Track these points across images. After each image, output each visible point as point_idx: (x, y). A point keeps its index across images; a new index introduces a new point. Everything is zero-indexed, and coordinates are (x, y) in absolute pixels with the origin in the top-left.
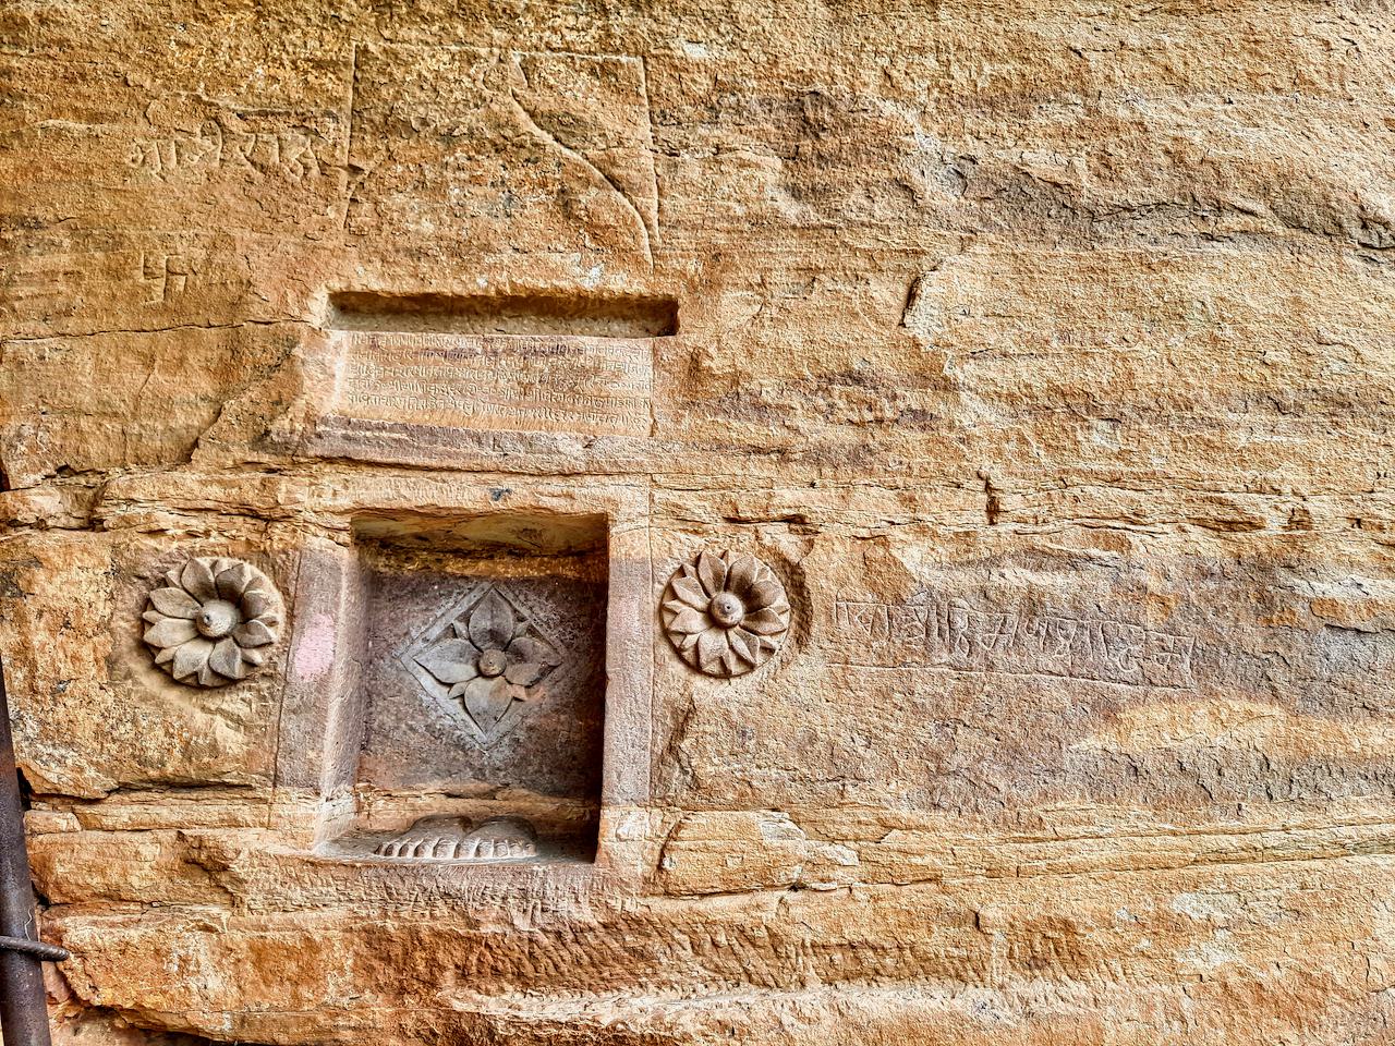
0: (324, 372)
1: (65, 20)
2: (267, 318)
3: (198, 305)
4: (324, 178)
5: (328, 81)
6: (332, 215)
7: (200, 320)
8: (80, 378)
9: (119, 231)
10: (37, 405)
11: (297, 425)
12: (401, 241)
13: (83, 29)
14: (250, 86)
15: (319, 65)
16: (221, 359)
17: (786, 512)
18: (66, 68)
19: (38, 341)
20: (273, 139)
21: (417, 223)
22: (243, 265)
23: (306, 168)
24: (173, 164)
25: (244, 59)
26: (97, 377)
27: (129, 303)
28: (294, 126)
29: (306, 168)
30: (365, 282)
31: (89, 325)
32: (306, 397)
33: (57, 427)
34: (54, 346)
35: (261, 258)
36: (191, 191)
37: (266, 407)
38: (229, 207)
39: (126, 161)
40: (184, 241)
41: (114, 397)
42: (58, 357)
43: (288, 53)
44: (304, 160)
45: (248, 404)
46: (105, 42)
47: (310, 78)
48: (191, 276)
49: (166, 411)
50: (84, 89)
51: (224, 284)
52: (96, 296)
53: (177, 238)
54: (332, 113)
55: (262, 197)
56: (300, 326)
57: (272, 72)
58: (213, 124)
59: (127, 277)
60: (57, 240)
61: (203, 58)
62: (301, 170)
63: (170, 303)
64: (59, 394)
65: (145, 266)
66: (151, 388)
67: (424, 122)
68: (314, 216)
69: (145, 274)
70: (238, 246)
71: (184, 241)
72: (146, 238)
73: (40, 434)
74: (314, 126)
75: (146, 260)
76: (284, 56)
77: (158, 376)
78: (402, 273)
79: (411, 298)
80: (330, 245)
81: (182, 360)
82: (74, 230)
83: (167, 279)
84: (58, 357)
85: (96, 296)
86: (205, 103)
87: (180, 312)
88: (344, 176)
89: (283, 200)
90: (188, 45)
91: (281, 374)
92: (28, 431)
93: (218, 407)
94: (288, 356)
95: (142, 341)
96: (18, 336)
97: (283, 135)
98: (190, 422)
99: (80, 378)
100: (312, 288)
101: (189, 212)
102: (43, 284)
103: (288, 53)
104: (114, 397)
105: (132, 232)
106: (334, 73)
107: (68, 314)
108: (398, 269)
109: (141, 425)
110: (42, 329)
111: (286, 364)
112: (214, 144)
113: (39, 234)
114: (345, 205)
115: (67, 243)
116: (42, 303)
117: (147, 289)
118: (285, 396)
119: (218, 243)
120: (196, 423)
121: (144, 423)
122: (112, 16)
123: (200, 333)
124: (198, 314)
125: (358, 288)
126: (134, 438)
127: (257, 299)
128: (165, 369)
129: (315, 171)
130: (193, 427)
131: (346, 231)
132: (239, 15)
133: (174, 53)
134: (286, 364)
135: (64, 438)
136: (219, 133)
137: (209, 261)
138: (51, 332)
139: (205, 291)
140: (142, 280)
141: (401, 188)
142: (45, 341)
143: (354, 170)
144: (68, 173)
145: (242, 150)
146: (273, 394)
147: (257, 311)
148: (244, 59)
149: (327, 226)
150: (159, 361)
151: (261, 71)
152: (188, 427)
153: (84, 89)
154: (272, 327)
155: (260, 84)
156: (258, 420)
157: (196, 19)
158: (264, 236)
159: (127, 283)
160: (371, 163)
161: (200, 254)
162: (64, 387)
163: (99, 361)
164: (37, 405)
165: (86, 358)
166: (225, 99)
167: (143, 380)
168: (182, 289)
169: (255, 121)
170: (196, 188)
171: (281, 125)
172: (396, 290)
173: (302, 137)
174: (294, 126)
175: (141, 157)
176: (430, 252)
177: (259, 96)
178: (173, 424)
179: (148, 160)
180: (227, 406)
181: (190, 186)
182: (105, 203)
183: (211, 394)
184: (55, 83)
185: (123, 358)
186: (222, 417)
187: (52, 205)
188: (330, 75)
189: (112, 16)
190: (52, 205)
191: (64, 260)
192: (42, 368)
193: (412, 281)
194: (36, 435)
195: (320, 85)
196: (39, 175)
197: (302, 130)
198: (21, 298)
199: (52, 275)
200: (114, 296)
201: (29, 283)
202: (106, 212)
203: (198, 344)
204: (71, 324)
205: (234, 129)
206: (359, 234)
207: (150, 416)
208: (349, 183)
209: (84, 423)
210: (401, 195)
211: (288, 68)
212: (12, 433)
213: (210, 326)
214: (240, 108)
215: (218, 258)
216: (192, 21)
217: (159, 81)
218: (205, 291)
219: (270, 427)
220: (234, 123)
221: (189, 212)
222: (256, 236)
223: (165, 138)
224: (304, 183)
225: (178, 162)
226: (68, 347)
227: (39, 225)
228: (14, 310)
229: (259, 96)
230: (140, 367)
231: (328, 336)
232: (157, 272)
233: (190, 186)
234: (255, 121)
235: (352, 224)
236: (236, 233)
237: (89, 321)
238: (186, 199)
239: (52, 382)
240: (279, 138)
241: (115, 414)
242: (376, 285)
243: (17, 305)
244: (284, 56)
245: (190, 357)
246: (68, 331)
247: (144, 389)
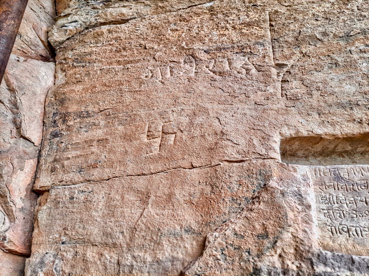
0: (302, 203)
1: (120, 30)
2: (240, 158)
3: (184, 153)
4: (260, 73)
5: (255, 30)
6: (271, 90)
7: (187, 164)
8: (94, 213)
9: (134, 112)
10: (60, 236)
11: (289, 263)
12: (330, 99)
13: (127, 32)
14: (210, 40)
15: (248, 25)
16: (202, 194)
17: (310, 267)
18: (117, 48)
19: (73, 186)
20: (225, 60)
21: (340, 87)
22: (216, 123)
23: (247, 70)
24: (168, 75)
25: (206, 30)
26: (106, 212)
27: (135, 156)
28: (237, 53)
29: (247, 70)
30: (309, 129)
31: (107, 172)
32: (291, 229)
33: (69, 256)
34: (81, 189)
35: (226, 117)
36: (179, 88)
37: (251, 240)
38: (202, 93)
39: (142, 77)
40: (175, 114)
41: (115, 229)
42: (82, 197)
43: (230, 24)
44: (246, 66)
45: (232, 237)
46: (137, 35)
47: (243, 31)
48: (179, 134)
49: (155, 242)
50: (124, 53)
51: (203, 136)
52: (115, 153)
53: (170, 112)
54: (260, 42)
55: (223, 86)
56: (268, 162)
57: (221, 32)
58: (191, 57)
59: (136, 139)
60: (97, 122)
61: (184, 33)
62: (244, 71)
63: (163, 154)
64: (77, 227)
65: (149, 131)
66: (144, 220)
67: (325, 34)
68: (259, 93)
69: (148, 136)
70: (210, 112)
71: (175, 114)
72: (150, 115)
73: (57, 261)
74: (249, 50)
75: (149, 127)
76: (228, 25)
77: (151, 210)
78: (339, 120)
79: (350, 139)
80: (275, 107)
81: (170, 196)
82: (108, 115)
83: (163, 138)
84: (82, 197)
85: (115, 153)
86: (186, 49)
87: (171, 158)
88: (274, 71)
89: (236, 86)
90: (177, 30)
91: (262, 206)
92: (49, 259)
93: (201, 239)
94: (265, 187)
95: (141, 183)
96: (61, 184)
97: (231, 57)
98: (175, 254)
99: (94, 213)
100: (271, 134)
101: (178, 98)
102: (84, 148)
103: (230, 24)
104: (115, 229)
105: (142, 113)
106: (257, 26)
107: (95, 167)
108: (335, 118)
109: (134, 257)
110: (77, 177)
111: (265, 196)
112: (191, 66)
113: (87, 120)
114: (279, 85)
115: (102, 123)
116: (80, 160)
117: (149, 145)
118: (270, 229)
119: (197, 112)
120: (180, 256)
121: (136, 254)
122: (141, 26)
123: (185, 173)
124: (184, 159)
125: (305, 134)
126: (126, 270)
127: (230, 143)
128: (157, 204)
129: (254, 71)
130: (178, 259)
131: (285, 98)
132: (201, 17)
133: (169, 34)
134: (265, 196)
135: (73, 267)
136: (194, 61)
137: (191, 123)
138: (81, 179)
139: (189, 143)
140: (146, 140)
141: (319, 69)
142: (77, 186)
143: (280, 66)
144: (109, 86)
145: (207, 67)
146: (257, 226)
147: (232, 153)
148: (206, 30)
149: (270, 97)
150: (153, 197)
151: (215, 33)
152: (173, 260)
153: (124, 53)
154: (245, 164)
155: (215, 38)
156: (245, 255)
157: (181, 21)
158: (227, 106)
159: (136, 143)
160: (292, 61)
161: (185, 120)
162: (81, 221)
163: (109, 199)
164: (60, 236)
165: (101, 196)
166: (197, 46)
167: (138, 214)
168: (172, 143)
169: (214, 53)
170: (182, 86)
171: (229, 53)
172: (338, 132)
173: (242, 58)
174: (237, 53)
175: (151, 74)
176: (360, 103)
177: (215, 43)
178: (160, 256)
179: (155, 75)
180: (211, 239)
181: (178, 85)
182: (128, 98)
183: (195, 226)
184: (111, 54)
185: (126, 196)
186: (208, 251)
187: (98, 104)
188: (255, 27)
189: (141, 26)
190: (98, 104)
191: (99, 133)
192: (70, 205)
193: (351, 124)
194: (54, 262)
195: (251, 33)
196: (94, 90)
197: (242, 54)
198: (69, 158)
199: (89, 143)
200: (126, 152)
201: (75, 149)
202: (128, 103)
203: (183, 182)
204: (96, 174)
205: (202, 58)
206: (295, 99)
207: (142, 247)
208: (278, 73)
209: (91, 254)
210: (319, 73)
211: (230, 30)
212: (38, 260)
213: (193, 167)
214: (206, 48)
215: (199, 120)
216: (179, 22)
217: (161, 46)
218: (189, 143)
219: (259, 264)
220: (202, 55)
221: (178, 98)
222: (221, 106)
223: (164, 66)
224: (249, 76)
225: (172, 75)
226: (90, 189)
227: (88, 115)
228: (63, 167)
229: (215, 43)
230: (137, 203)
231: (295, 171)
232: (156, 134)
233: (178, 85)
234: (214, 53)
235: (288, 94)
236: (209, 106)
237: (107, 170)
238: (176, 92)
239: (74, 217)
240: (228, 59)
241: (115, 245)
242: (319, 131)
243: (66, 163)
244: (228, 25)
245: (177, 192)
246: (93, 178)
247: (139, 222)
